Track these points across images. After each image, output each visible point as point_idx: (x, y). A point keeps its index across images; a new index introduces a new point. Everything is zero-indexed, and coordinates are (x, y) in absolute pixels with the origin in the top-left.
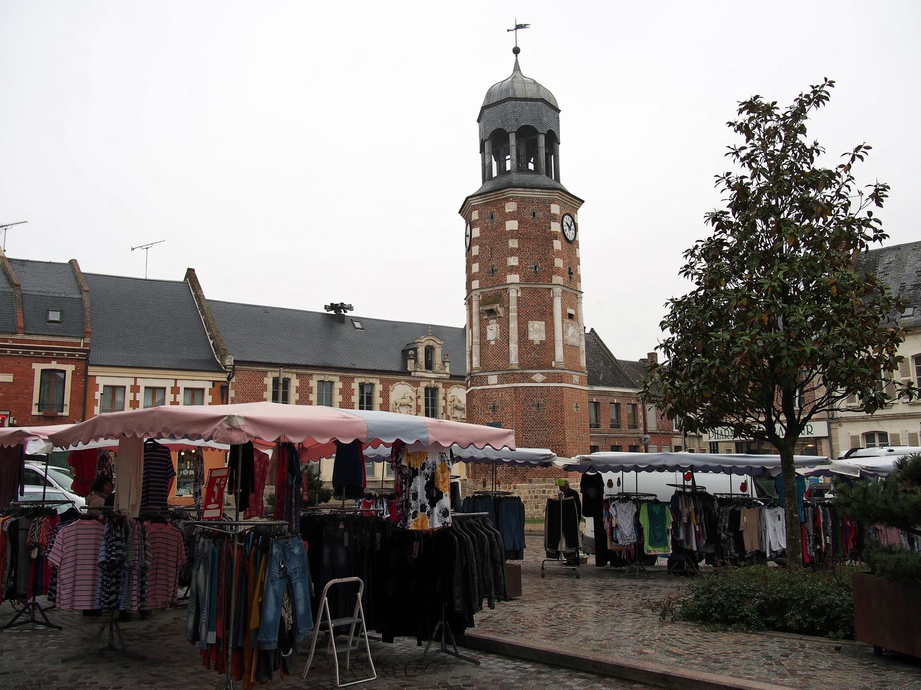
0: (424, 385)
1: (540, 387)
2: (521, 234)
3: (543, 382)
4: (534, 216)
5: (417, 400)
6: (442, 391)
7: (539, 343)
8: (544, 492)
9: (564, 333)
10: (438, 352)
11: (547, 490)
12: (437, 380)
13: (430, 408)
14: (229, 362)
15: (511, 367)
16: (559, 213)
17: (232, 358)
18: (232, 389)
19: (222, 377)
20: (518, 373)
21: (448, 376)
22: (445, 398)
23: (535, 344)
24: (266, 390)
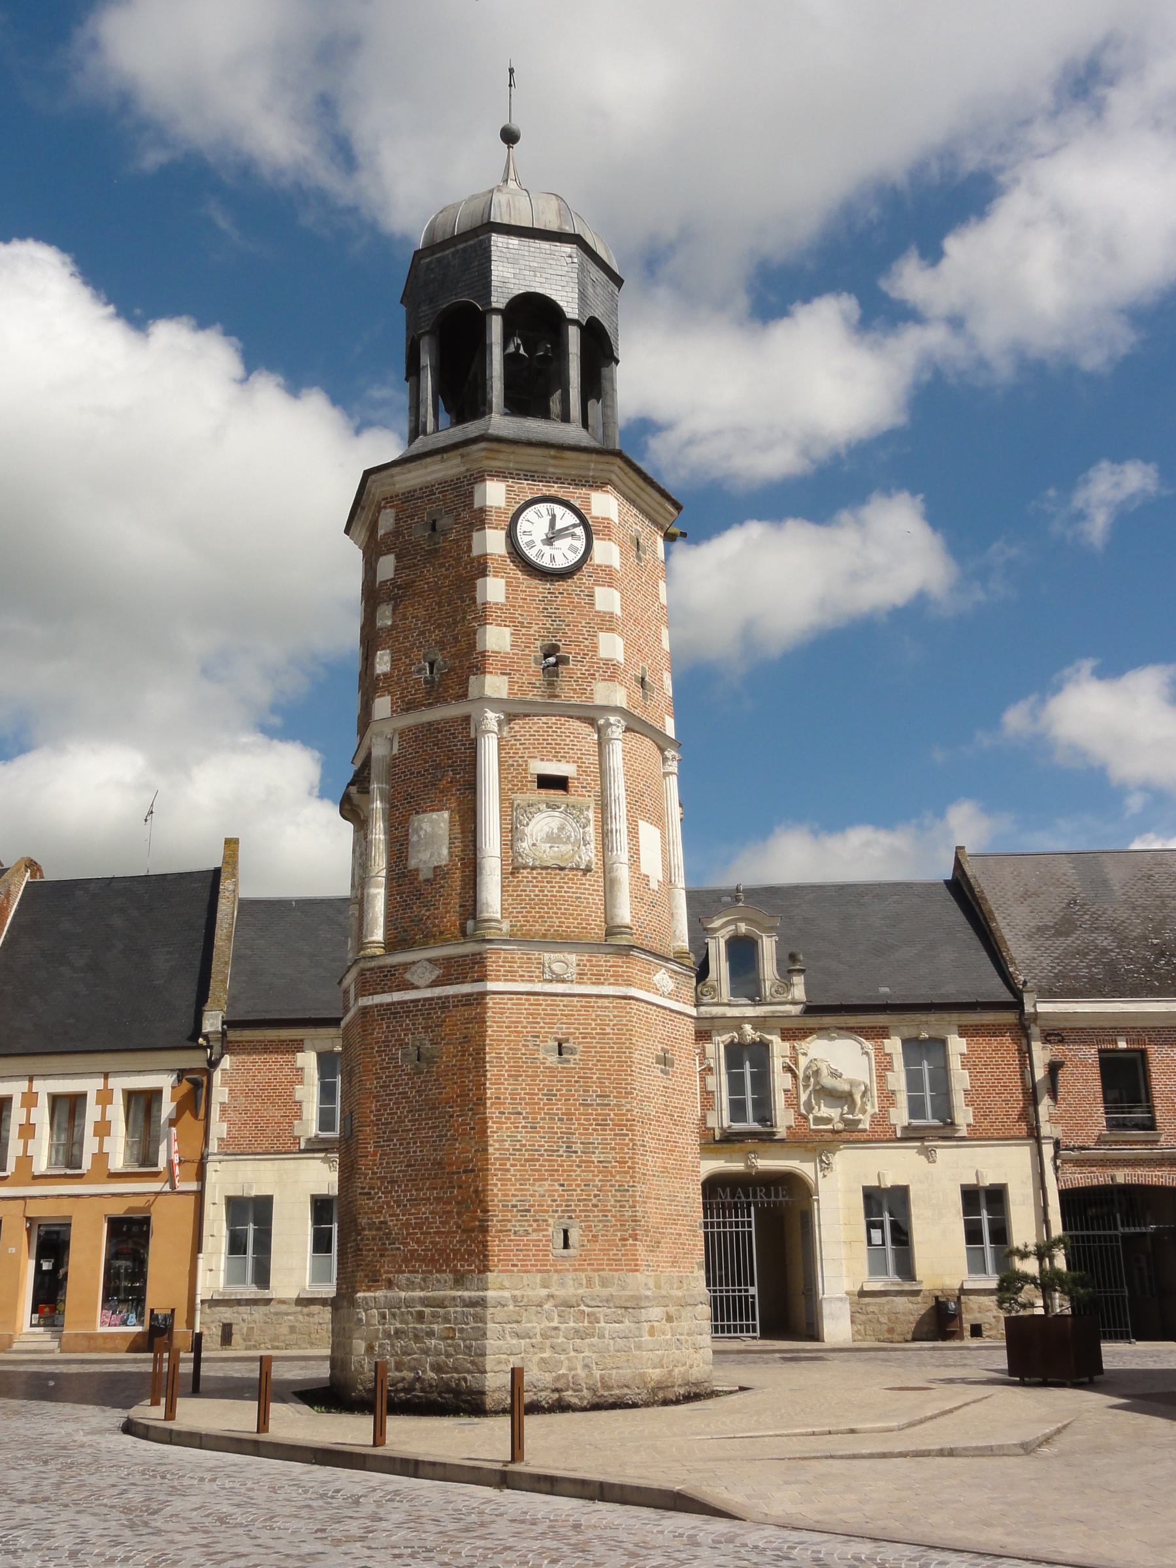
0: (723, 1039)
1: (425, 1000)
2: (399, 587)
3: (434, 984)
4: (434, 528)
5: (703, 1079)
6: (779, 1048)
7: (431, 876)
8: (420, 1317)
9: (512, 833)
10: (768, 947)
11: (427, 1310)
12: (759, 1023)
13: (749, 1096)
14: (212, 1025)
15: (369, 952)
16: (503, 504)
17: (217, 1016)
18: (223, 1084)
19: (194, 1060)
20: (371, 969)
21: (795, 1010)
22: (788, 1069)
23: (421, 877)
24: (301, 1082)
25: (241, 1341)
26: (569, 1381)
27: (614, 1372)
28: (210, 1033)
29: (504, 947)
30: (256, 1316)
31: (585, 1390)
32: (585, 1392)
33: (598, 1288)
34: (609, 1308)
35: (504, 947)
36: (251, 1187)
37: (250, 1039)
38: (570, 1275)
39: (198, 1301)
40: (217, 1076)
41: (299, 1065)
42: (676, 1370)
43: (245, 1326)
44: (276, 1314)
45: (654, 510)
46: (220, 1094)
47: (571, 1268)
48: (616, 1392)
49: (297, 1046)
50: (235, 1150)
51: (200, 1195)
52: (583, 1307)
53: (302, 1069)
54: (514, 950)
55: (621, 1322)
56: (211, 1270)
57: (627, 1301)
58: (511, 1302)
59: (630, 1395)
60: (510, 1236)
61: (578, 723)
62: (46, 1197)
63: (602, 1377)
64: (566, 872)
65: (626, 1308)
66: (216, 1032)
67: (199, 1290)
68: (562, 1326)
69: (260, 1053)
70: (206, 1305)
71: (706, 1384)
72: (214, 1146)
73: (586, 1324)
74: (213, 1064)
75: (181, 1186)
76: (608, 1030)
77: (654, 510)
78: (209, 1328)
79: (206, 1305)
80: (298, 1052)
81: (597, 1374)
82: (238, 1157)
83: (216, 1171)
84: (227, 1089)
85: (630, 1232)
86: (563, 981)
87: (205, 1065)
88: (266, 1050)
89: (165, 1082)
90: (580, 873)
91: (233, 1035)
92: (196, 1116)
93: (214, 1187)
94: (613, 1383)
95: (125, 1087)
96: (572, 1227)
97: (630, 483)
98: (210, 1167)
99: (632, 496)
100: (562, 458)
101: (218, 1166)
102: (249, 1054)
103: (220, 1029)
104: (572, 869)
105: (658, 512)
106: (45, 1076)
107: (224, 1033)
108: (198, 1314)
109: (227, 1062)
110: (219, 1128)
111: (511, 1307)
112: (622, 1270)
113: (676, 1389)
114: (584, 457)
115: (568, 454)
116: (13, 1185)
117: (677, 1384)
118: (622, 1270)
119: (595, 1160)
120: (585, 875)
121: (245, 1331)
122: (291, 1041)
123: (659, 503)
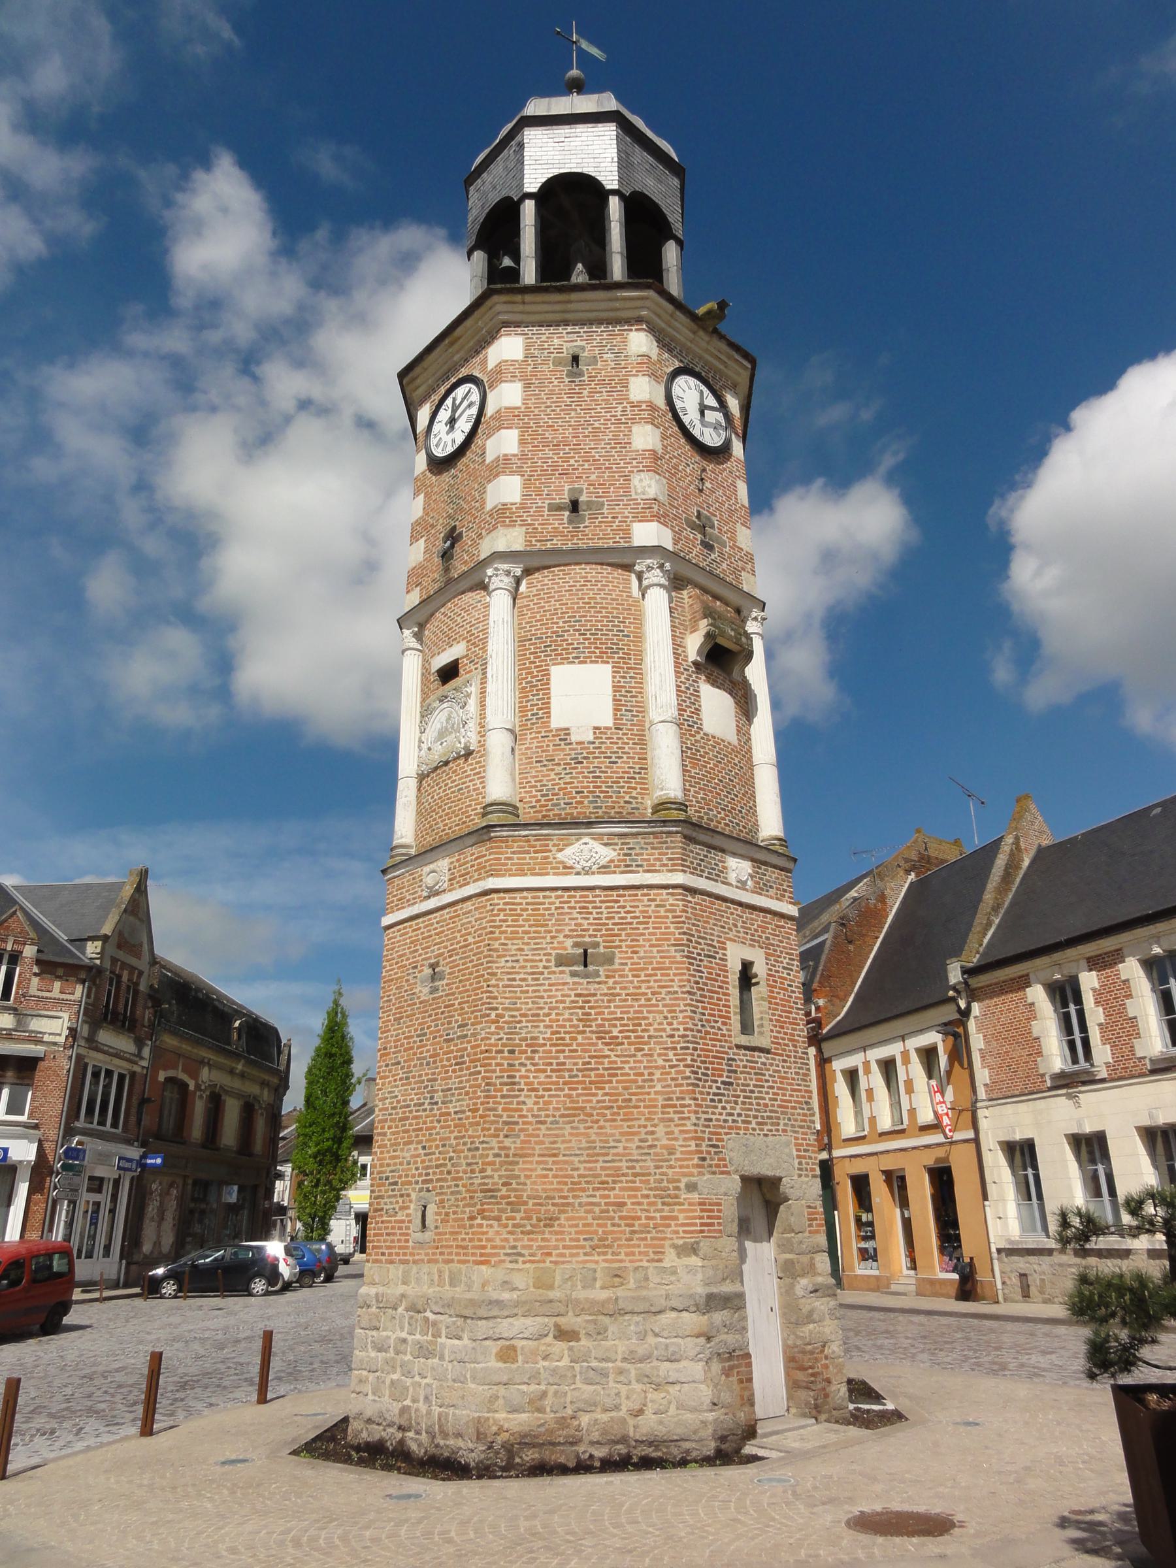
19: (948, 1013)
25: (1037, 1294)
26: (411, 1418)
27: (451, 1410)
28: (955, 984)
29: (395, 874)
30: (1045, 1267)
31: (424, 1433)
32: (424, 1437)
33: (447, 1287)
34: (450, 1316)
35: (395, 874)
36: (1014, 1132)
37: (988, 983)
38: (425, 1268)
39: (994, 1250)
40: (972, 1025)
41: (1029, 1001)
42: (585, 1419)
43: (1037, 1277)
44: (1061, 1265)
45: (611, 310)
46: (977, 1042)
47: (426, 1258)
48: (451, 1442)
49: (1023, 983)
50: (1001, 1095)
51: (976, 1141)
52: (429, 1314)
53: (1033, 1004)
54: (403, 874)
55: (459, 1338)
56: (1000, 1218)
57: (466, 1307)
58: (374, 1302)
59: (470, 1451)
60: (381, 1216)
61: (470, 594)
62: (888, 1152)
63: (440, 1415)
64: (451, 765)
65: (466, 1317)
66: (959, 983)
67: (992, 1240)
68: (410, 1338)
69: (998, 995)
70: (1003, 1254)
71: (687, 1445)
72: (982, 1093)
73: (430, 1338)
74: (966, 1013)
75: (958, 1136)
76: (471, 940)
77: (611, 310)
78: (1009, 1278)
79: (1003, 1254)
80: (1027, 987)
81: (436, 1410)
82: (999, 1102)
83: (986, 1117)
84: (981, 1035)
85: (479, 1207)
86: (437, 893)
87: (957, 1016)
88: (1003, 992)
89: (933, 1038)
90: (462, 761)
91: (978, 981)
92: (962, 1066)
93: (987, 1133)
94: (450, 1430)
95: (918, 1046)
96: (430, 1203)
97: (587, 306)
98: (981, 1113)
99: (558, 317)
100: (459, 338)
101: (986, 1112)
102: (991, 998)
103: (961, 979)
104: (455, 759)
105: (618, 309)
106: (872, 1046)
107: (966, 983)
108: (996, 1263)
109: (976, 1008)
110: (982, 1075)
111: (374, 1309)
112: (468, 1261)
113: (581, 1449)
114: (468, 323)
115: (459, 331)
116: (870, 1143)
117: (586, 1440)
118: (468, 1261)
119: (452, 1110)
120: (466, 760)
121: (1038, 1282)
122: (1020, 977)
123: (610, 300)
